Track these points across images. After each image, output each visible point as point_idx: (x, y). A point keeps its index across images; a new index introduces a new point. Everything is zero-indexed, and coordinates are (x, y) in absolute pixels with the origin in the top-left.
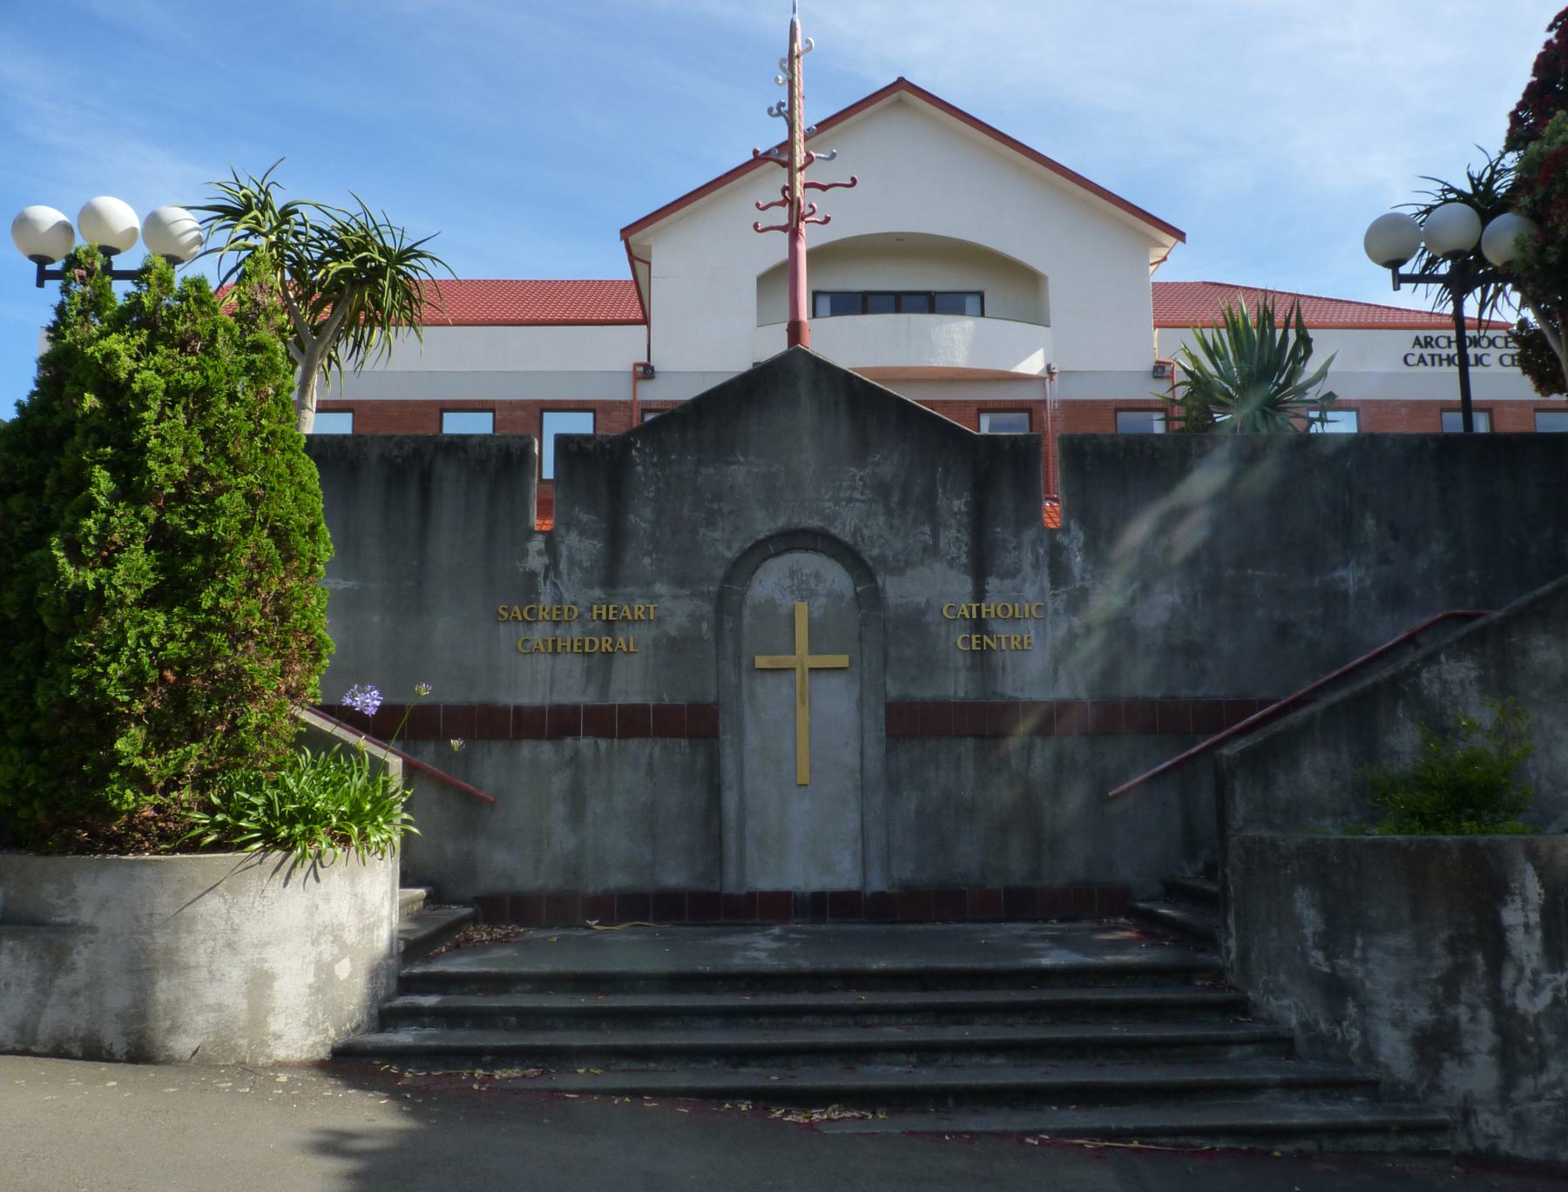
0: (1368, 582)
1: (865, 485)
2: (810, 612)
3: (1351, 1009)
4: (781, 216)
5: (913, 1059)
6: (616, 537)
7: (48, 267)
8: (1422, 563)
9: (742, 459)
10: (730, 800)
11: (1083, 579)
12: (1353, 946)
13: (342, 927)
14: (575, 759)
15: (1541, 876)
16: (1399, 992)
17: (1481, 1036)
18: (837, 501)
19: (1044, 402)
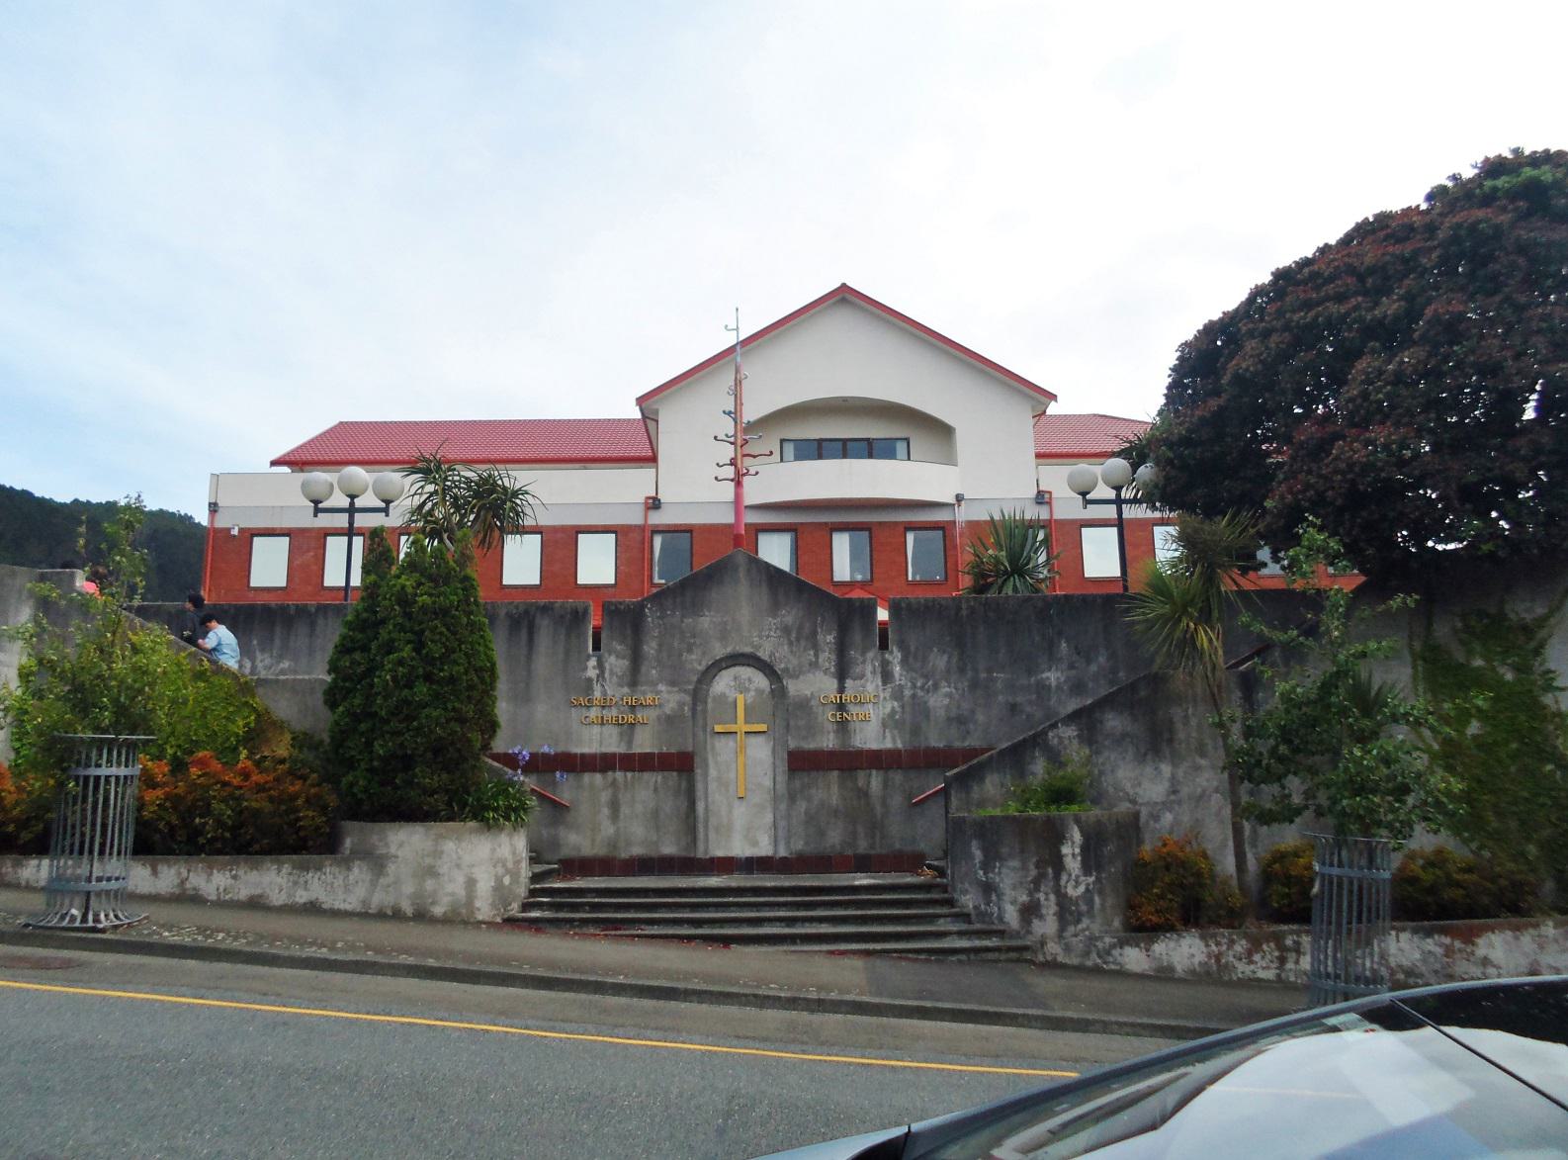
0: (1062, 679)
1: (777, 629)
2: (745, 701)
3: (994, 897)
4: (730, 472)
5: (783, 924)
6: (636, 659)
7: (320, 506)
8: (1093, 668)
9: (707, 613)
10: (700, 807)
11: (900, 680)
12: (995, 867)
13: (506, 859)
14: (614, 783)
15: (1081, 831)
16: (1014, 888)
17: (1050, 907)
18: (760, 637)
19: (954, 522)
